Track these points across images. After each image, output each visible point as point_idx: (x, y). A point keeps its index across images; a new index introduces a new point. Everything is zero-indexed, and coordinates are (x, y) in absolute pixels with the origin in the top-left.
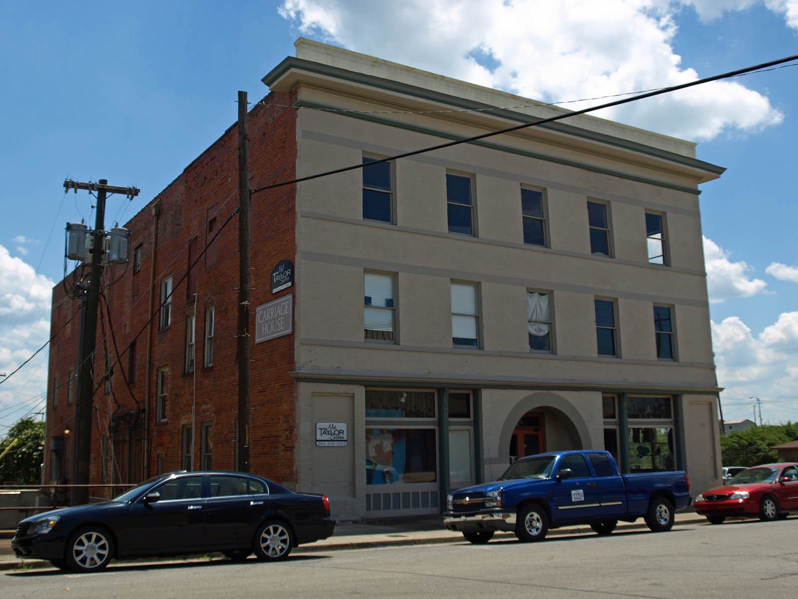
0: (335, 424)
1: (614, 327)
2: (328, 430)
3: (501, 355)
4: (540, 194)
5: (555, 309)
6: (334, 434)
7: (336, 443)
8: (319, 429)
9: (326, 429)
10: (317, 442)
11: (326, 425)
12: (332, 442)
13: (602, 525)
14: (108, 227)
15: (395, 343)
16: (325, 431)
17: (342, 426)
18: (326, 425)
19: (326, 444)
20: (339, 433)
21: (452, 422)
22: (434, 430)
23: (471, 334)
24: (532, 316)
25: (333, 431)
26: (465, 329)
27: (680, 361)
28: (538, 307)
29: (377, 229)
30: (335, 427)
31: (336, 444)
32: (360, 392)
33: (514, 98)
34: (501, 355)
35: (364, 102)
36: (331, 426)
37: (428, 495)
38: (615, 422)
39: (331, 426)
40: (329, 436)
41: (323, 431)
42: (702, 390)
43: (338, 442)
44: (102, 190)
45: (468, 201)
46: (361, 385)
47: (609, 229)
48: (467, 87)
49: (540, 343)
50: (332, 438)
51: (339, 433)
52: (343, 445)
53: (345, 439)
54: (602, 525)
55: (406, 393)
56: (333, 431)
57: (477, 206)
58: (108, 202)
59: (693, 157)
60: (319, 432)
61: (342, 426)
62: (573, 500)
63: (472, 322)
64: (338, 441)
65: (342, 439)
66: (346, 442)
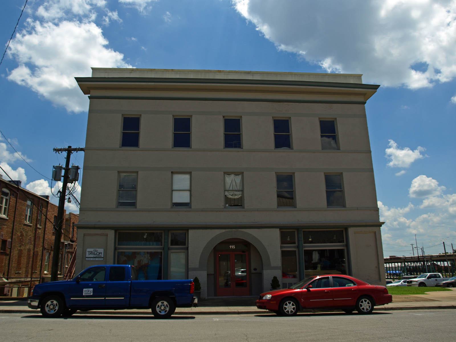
0: (97, 249)
1: (341, 189)
2: (93, 252)
3: (203, 210)
4: (288, 121)
5: (344, 183)
6: (96, 254)
7: (97, 258)
8: (88, 252)
9: (92, 252)
10: (86, 258)
11: (92, 250)
12: (95, 258)
13: (70, 310)
14: (70, 167)
15: (344, 207)
16: (91, 253)
17: (101, 250)
18: (92, 250)
19: (92, 259)
20: (99, 254)
21: (306, 246)
22: (295, 251)
23: (187, 200)
24: (230, 187)
25: (96, 253)
26: (182, 197)
27: (347, 206)
28: (234, 182)
29: (233, 152)
30: (97, 251)
31: (97, 259)
32: (111, 234)
33: (220, 72)
34: (203, 210)
35: (238, 93)
36: (95, 250)
37: (287, 285)
38: (344, 245)
39: (95, 250)
40: (94, 255)
41: (90, 253)
42: (364, 224)
43: (98, 258)
44: (69, 151)
45: (239, 131)
46: (112, 230)
47: (290, 133)
48: (188, 72)
49: (236, 204)
50: (95, 256)
51: (99, 254)
52: (101, 260)
53: (103, 257)
54: (70, 310)
55: (147, 233)
56: (96, 253)
57: (292, 133)
58: (72, 156)
59: (361, 83)
60: (87, 253)
61: (101, 250)
62: (84, 294)
63: (188, 194)
64: (98, 258)
65: (101, 257)
66: (103, 259)
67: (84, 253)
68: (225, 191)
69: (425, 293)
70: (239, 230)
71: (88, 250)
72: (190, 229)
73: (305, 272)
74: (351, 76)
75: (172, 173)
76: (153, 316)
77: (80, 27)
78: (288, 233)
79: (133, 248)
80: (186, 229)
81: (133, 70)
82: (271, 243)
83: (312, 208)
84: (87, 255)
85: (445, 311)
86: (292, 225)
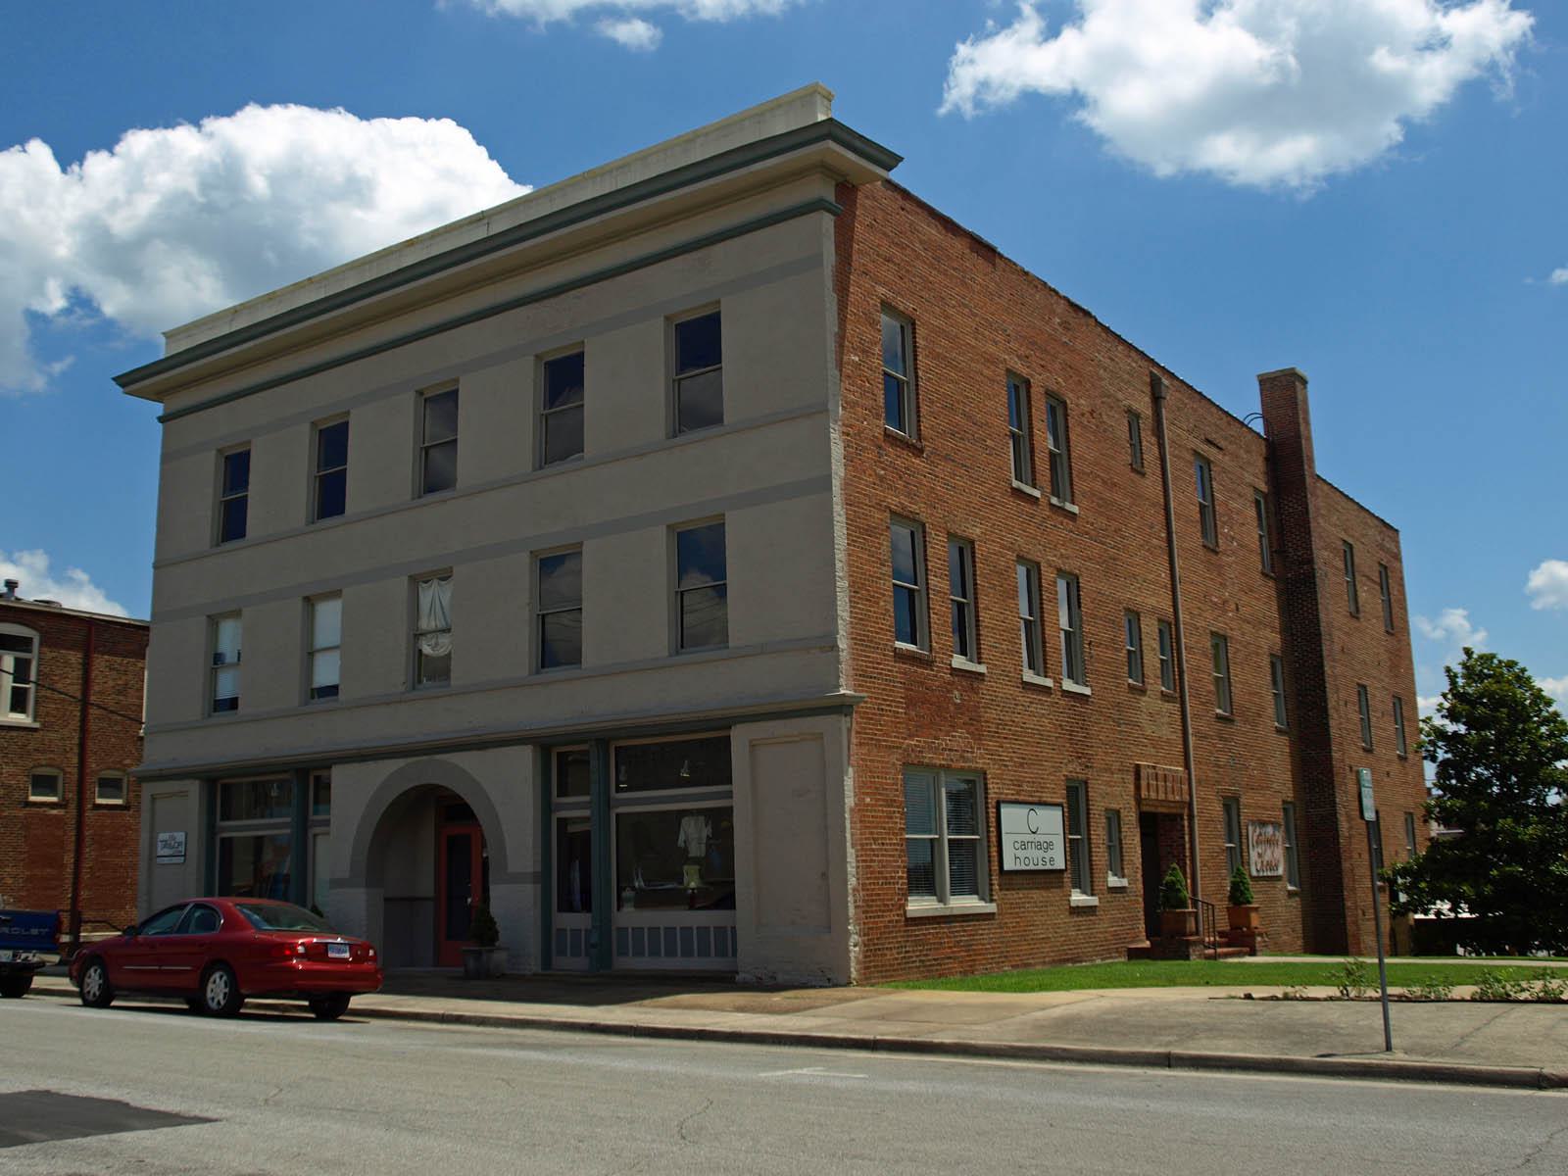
16: (166, 844)
32: (194, 788)
67: (152, 845)
68: (415, 635)
69: (340, 1018)
70: (438, 757)
71: (163, 836)
72: (335, 763)
73: (949, 840)
74: (383, 256)
75: (417, 581)
76: (313, 1016)
77: (1073, 82)
78: (565, 759)
79: (249, 826)
80: (327, 763)
81: (236, 311)
82: (508, 794)
83: (633, 672)
84: (161, 852)
85: (656, 1046)
86: (579, 727)
